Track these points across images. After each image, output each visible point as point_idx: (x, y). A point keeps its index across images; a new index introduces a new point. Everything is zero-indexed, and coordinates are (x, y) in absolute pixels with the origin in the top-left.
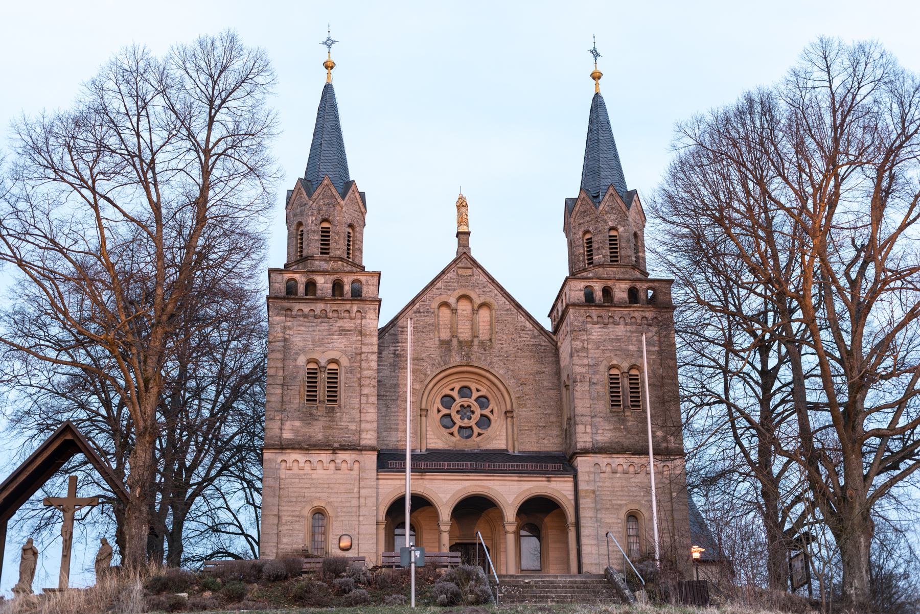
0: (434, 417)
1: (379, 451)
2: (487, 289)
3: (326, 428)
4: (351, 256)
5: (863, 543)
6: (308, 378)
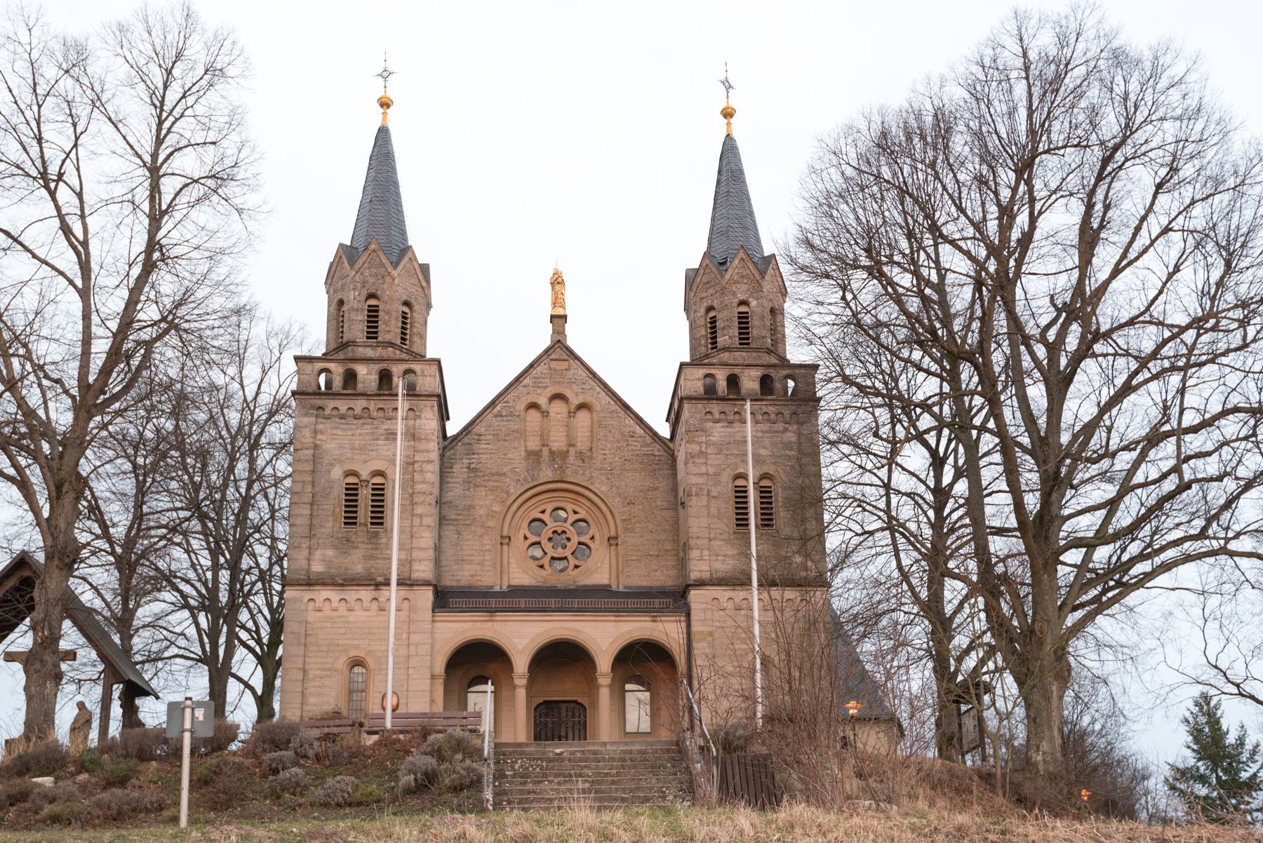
1: (435, 586)
2: (587, 387)
4: (408, 342)
5: (1055, 693)
6: (346, 495)
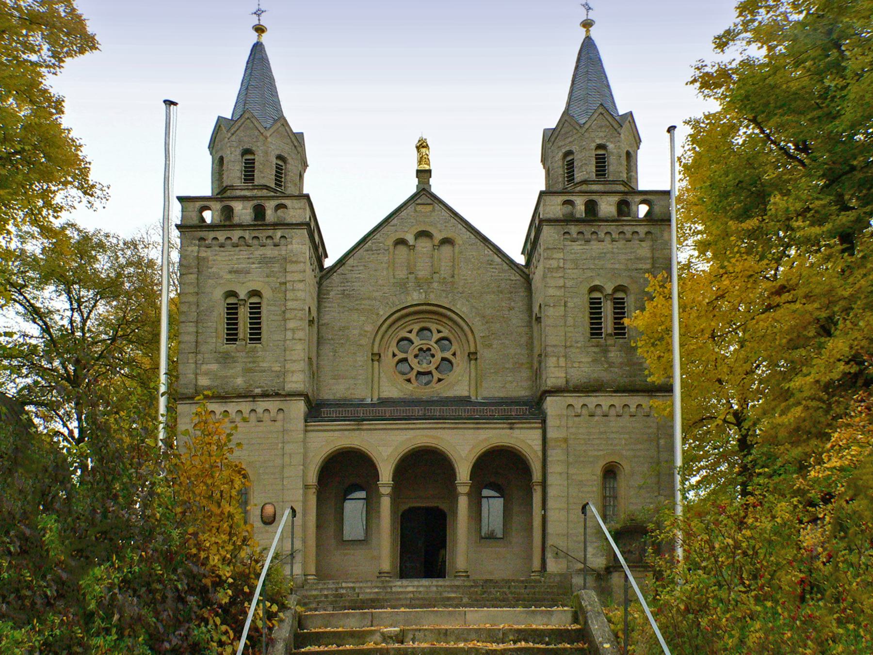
0: (388, 361)
3: (247, 371)
